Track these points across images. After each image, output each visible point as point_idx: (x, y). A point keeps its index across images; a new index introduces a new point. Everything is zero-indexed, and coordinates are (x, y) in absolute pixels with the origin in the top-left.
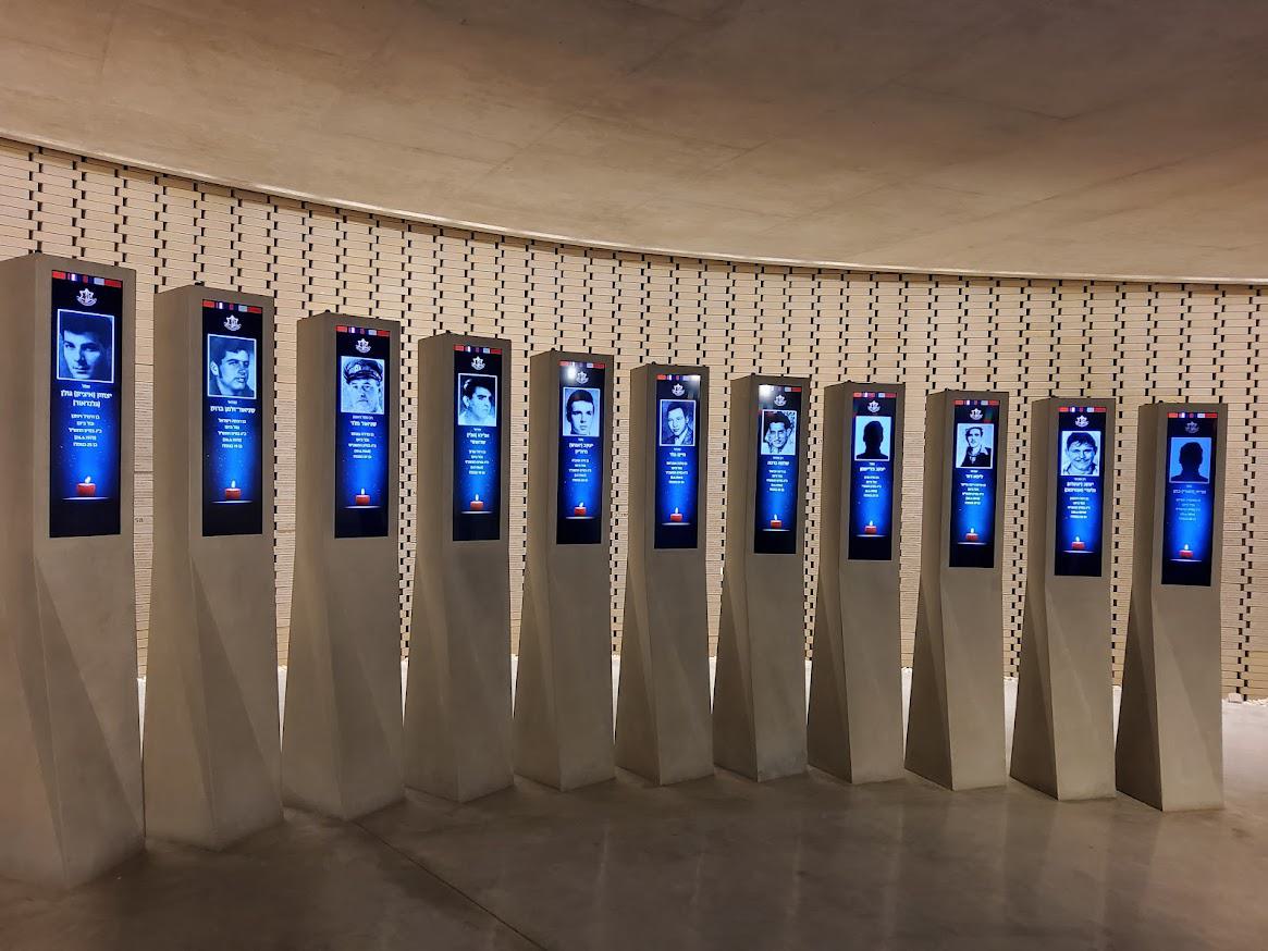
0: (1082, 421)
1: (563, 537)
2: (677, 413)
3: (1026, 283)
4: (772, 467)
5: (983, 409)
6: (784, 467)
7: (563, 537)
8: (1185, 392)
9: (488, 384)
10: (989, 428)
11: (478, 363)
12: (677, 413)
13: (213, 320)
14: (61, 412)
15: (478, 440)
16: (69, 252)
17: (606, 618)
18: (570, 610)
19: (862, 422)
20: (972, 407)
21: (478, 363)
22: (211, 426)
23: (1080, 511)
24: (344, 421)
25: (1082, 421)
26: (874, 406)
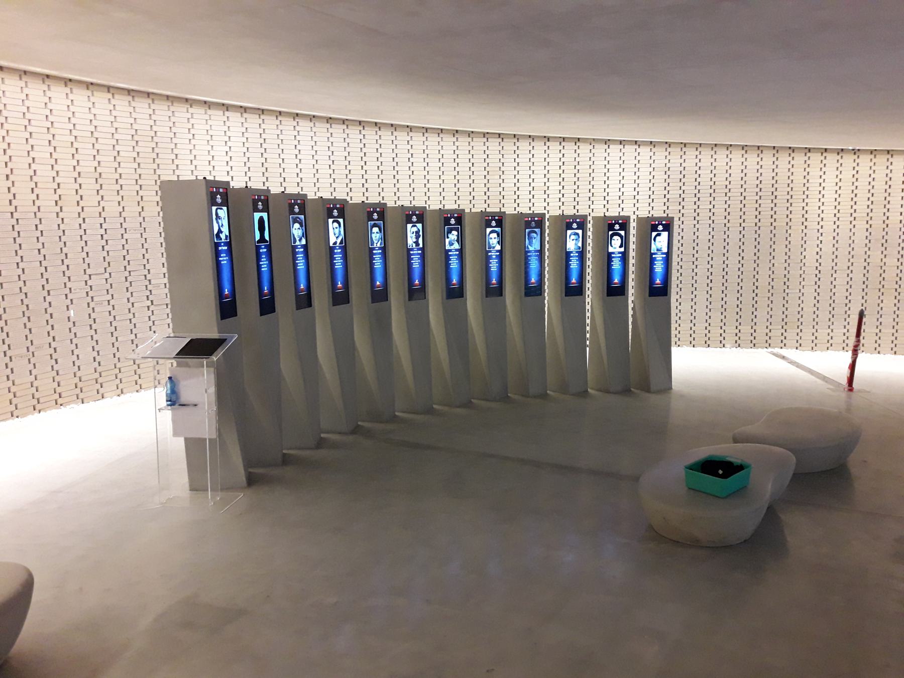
0: (617, 227)
1: (374, 300)
2: (297, 225)
3: (243, 110)
4: (413, 254)
5: (578, 223)
6: (418, 254)
7: (374, 300)
8: (667, 212)
9: (457, 230)
10: (665, 235)
11: (453, 221)
12: (376, 230)
13: (528, 225)
14: (217, 254)
15: (659, 257)
16: (574, 212)
17: (584, 325)
18: (574, 322)
19: (257, 216)
20: (573, 222)
21: (453, 221)
22: (217, 254)
23: (659, 268)
24: (568, 254)
25: (617, 227)
26: (575, 226)
